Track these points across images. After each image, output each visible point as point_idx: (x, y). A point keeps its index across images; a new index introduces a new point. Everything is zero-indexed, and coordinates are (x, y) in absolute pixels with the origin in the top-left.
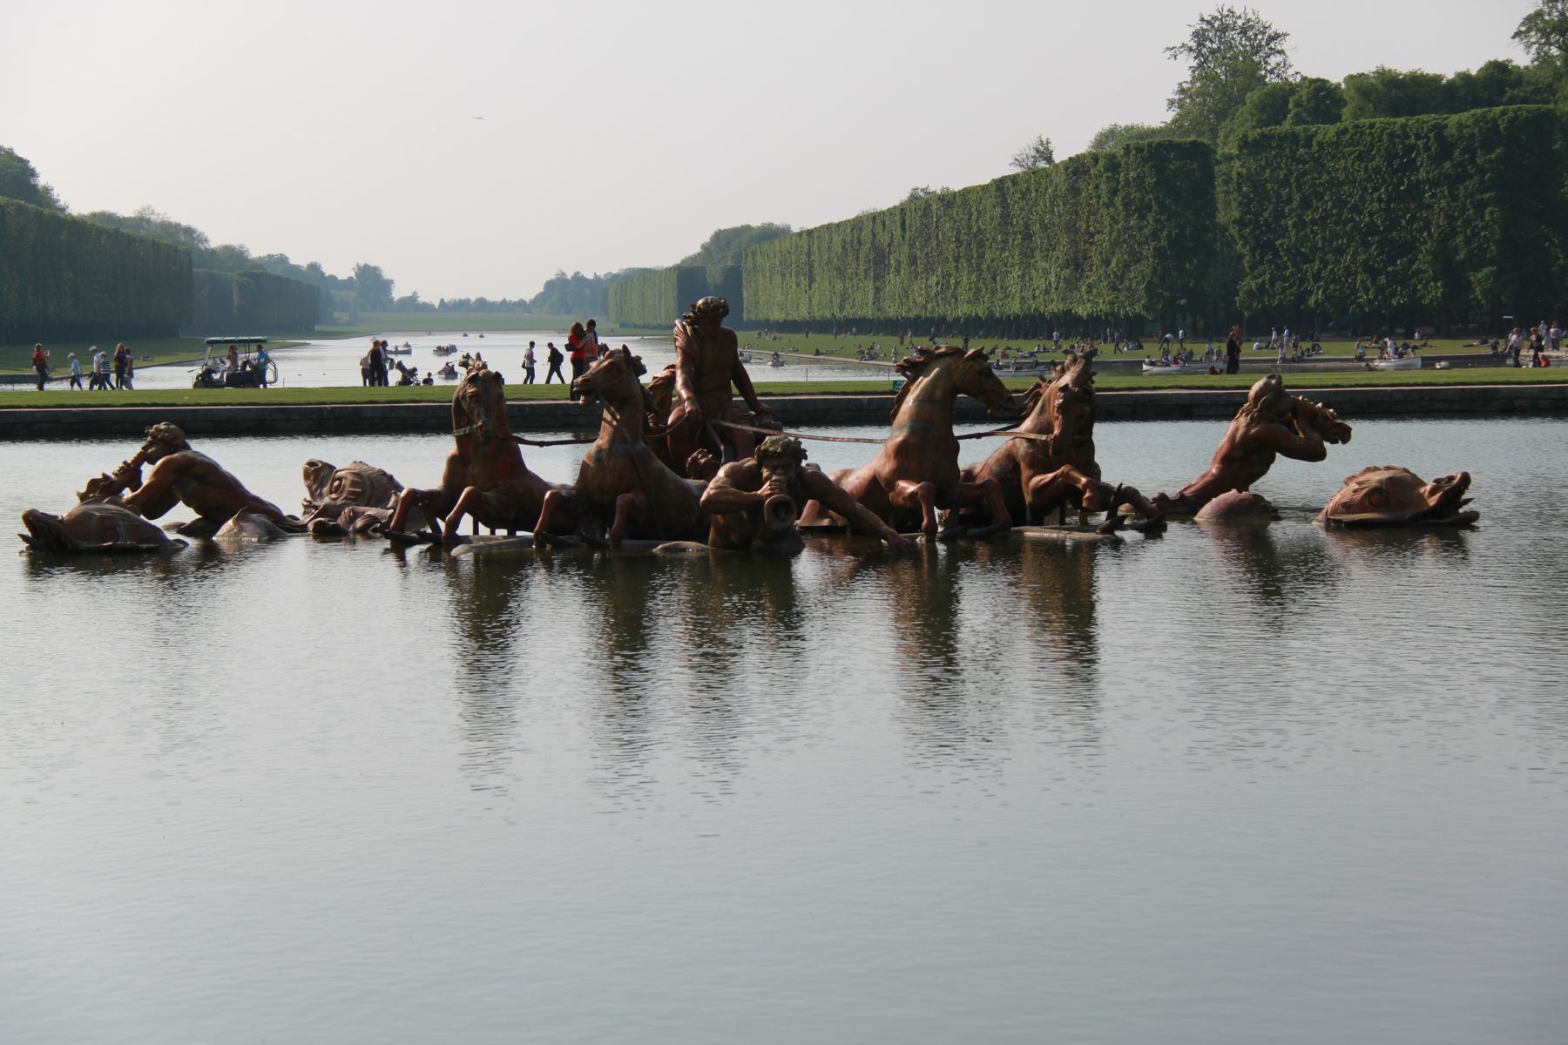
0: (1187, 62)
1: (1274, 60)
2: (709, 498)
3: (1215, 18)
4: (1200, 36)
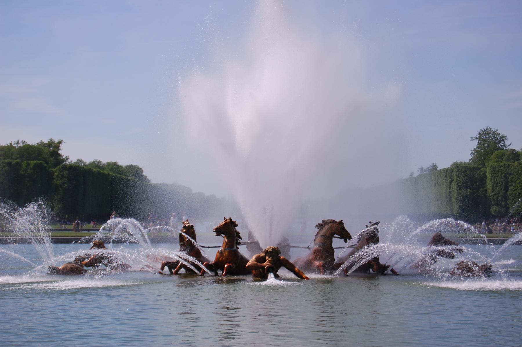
0: (475, 143)
2: (248, 266)
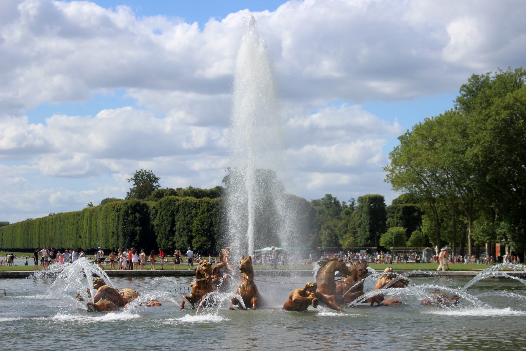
4: (136, 176)
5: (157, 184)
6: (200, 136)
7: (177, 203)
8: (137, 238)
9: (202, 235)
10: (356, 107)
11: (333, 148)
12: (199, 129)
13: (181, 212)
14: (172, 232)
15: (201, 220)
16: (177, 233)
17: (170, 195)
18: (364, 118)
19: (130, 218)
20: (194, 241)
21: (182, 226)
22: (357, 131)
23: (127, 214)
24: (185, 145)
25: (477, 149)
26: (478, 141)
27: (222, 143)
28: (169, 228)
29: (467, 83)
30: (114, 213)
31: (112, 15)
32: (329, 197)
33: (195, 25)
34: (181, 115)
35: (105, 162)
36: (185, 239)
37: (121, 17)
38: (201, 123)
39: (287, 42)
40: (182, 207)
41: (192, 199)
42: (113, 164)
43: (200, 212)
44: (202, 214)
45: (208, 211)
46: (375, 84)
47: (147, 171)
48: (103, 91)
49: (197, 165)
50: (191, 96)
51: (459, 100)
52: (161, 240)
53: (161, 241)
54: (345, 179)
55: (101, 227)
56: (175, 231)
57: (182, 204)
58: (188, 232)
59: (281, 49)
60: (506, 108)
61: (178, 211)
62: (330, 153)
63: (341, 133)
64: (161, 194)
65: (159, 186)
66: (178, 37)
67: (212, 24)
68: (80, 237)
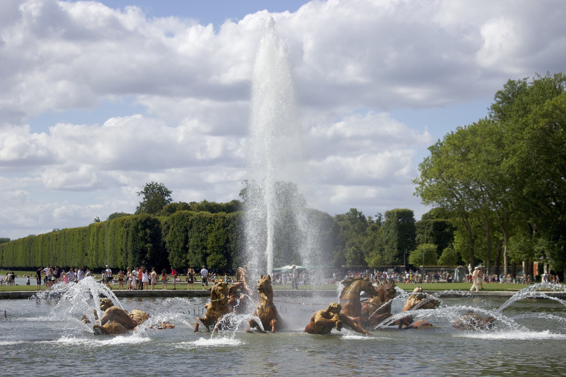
1: (167, 198)
3: (151, 185)
4: (147, 189)
5: (169, 197)
6: (215, 146)
7: (191, 218)
8: (148, 255)
9: (217, 252)
10: (384, 114)
11: (359, 159)
12: (215, 138)
13: (194, 228)
14: (185, 250)
15: (216, 236)
16: (190, 250)
17: (183, 209)
18: (392, 128)
19: (140, 234)
20: (208, 259)
21: (195, 243)
22: (384, 141)
23: (137, 230)
24: (199, 156)
25: (513, 161)
26: (515, 151)
27: (239, 153)
28: (181, 245)
29: (502, 89)
30: (122, 229)
31: (120, 16)
32: (354, 211)
33: (210, 27)
34: (194, 123)
35: (113, 174)
36: (199, 257)
37: (131, 18)
38: (217, 133)
39: (309, 45)
40: (195, 222)
41: (207, 214)
42: (122, 177)
43: (215, 227)
44: (218, 229)
45: (224, 226)
46: (403, 91)
47: (159, 184)
48: (111, 98)
49: (212, 177)
50: (206, 103)
51: (494, 107)
52: (173, 258)
53: (174, 259)
54: (371, 192)
55: (108, 244)
56: (188, 248)
57: (196, 219)
58: (202, 249)
59: (302, 52)
60: (544, 116)
61: (191, 227)
62: (356, 164)
63: (367, 143)
64: (173, 208)
65: (171, 200)
66: (192, 40)
67: (228, 26)
68: (86, 255)
